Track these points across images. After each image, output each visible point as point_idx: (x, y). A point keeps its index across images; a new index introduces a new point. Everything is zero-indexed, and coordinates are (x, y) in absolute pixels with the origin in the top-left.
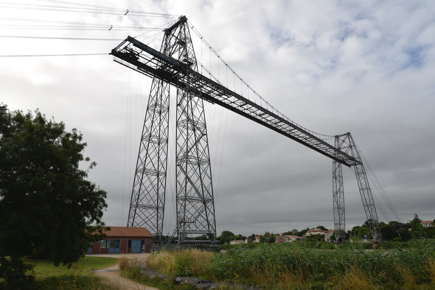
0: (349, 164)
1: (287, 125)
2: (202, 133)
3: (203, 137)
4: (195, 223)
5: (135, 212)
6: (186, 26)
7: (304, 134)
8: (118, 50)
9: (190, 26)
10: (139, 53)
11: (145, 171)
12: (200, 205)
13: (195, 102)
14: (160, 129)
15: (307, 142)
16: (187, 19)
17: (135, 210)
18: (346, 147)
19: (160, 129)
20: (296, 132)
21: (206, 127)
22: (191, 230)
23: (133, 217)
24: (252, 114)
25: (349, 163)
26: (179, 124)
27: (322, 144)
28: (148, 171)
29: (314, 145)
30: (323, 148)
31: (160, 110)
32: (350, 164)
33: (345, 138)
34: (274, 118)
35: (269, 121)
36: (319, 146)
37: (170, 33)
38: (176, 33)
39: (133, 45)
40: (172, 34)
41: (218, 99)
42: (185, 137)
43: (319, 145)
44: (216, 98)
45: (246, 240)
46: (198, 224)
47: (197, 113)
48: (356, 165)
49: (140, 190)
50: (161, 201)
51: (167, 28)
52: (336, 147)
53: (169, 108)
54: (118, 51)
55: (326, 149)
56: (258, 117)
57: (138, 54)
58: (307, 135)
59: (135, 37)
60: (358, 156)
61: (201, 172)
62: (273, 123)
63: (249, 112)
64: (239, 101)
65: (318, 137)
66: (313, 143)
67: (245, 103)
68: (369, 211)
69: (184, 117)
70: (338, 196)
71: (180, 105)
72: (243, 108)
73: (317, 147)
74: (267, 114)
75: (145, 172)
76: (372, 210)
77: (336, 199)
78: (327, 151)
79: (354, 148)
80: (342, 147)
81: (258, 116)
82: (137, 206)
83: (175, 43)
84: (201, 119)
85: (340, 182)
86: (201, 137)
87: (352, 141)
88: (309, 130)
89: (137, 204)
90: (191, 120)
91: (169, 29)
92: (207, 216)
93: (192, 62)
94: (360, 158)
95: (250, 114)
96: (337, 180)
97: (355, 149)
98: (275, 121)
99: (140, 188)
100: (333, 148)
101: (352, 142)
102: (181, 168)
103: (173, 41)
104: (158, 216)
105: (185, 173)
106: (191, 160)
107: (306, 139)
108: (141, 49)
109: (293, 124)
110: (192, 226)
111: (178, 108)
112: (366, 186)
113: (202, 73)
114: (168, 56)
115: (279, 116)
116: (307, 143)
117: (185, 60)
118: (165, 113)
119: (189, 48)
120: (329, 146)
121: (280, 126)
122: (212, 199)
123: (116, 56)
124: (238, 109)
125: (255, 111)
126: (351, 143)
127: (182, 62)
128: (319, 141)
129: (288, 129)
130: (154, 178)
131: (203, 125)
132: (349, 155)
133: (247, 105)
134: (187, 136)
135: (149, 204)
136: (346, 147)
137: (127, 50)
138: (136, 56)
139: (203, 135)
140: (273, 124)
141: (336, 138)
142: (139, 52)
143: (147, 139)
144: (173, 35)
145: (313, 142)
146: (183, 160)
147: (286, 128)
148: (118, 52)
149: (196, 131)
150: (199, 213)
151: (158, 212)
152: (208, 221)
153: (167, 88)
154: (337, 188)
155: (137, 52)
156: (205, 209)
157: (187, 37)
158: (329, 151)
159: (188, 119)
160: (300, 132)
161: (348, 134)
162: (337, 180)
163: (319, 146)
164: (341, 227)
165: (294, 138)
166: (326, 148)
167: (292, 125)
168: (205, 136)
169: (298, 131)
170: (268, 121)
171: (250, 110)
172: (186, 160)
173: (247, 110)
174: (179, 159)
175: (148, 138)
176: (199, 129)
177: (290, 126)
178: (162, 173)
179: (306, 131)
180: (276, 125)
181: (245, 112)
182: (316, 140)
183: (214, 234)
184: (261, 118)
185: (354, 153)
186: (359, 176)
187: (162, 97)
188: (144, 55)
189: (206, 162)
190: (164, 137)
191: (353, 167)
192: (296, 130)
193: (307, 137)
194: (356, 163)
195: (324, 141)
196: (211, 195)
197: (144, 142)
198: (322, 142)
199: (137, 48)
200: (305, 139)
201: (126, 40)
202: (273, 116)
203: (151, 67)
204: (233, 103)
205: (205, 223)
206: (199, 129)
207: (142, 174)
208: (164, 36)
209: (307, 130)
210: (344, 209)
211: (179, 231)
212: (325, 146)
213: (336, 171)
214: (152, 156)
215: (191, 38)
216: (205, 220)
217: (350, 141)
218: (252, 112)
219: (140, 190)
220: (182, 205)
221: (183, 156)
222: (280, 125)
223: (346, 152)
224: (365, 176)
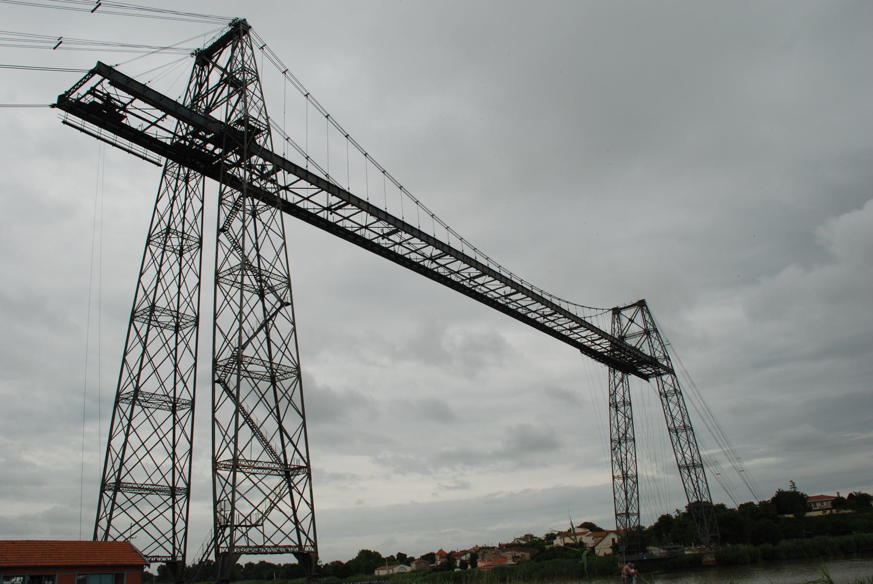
0: (645, 374)
1: (497, 282)
2: (281, 301)
3: (282, 310)
4: (260, 528)
5: (114, 503)
6: (248, 43)
7: (539, 304)
8: (74, 96)
9: (257, 44)
10: (125, 105)
11: (171, 405)
12: (274, 481)
13: (263, 223)
14: (179, 292)
15: (547, 324)
16: (250, 27)
17: (112, 498)
18: (637, 335)
19: (179, 292)
20: (521, 299)
21: (289, 286)
22: (251, 544)
23: (108, 516)
24: (413, 256)
25: (645, 370)
26: (221, 278)
27: (582, 328)
28: (147, 399)
29: (564, 330)
30: (585, 337)
31: (182, 246)
32: (647, 373)
33: (635, 313)
34: (466, 266)
35: (455, 272)
36: (577, 333)
37: (209, 61)
38: (223, 59)
39: (109, 83)
40: (212, 62)
41: (327, 218)
42: (237, 310)
43: (575, 331)
44: (321, 215)
45: (413, 565)
46: (268, 528)
47: (267, 252)
48: (660, 375)
49: (125, 445)
50: (180, 474)
51: (202, 48)
52: (616, 334)
53: (201, 239)
54: (74, 99)
55: (593, 339)
56: (427, 264)
57: (124, 107)
58: (547, 307)
59: (117, 65)
60: (664, 355)
61: (279, 397)
62: (464, 278)
63: (405, 251)
64: (380, 224)
65: (573, 310)
66: (561, 325)
67: (393, 229)
68: (692, 479)
69: (235, 260)
70: (623, 450)
71: (226, 230)
72: (389, 240)
73: (571, 336)
74: (448, 257)
75: (138, 400)
76: (697, 478)
77: (619, 456)
78: (596, 344)
79: (655, 335)
80: (627, 334)
81: (428, 261)
82: (118, 486)
83: (221, 81)
84: (278, 265)
85: (625, 416)
86: (278, 310)
87: (651, 319)
88: (550, 296)
89: (118, 481)
90: (254, 267)
91: (206, 49)
92: (293, 508)
93: (258, 127)
94: (669, 360)
95: (407, 256)
96: (619, 412)
97: (657, 338)
98: (469, 274)
99: (126, 441)
100: (609, 338)
101: (649, 321)
102: (226, 389)
103: (215, 77)
104: (174, 512)
105: (236, 399)
106: (250, 368)
107: (545, 316)
108: (129, 94)
109: (513, 279)
110: (253, 533)
111: (220, 238)
112: (684, 422)
113: (307, 167)
114: (201, 112)
115: (478, 260)
116: (548, 327)
117: (239, 122)
118: (192, 252)
119: (253, 94)
120: (598, 332)
121: (483, 285)
122: (305, 465)
123: (102, 128)
124: (410, 258)
125: (420, 249)
126: (648, 325)
127: (234, 125)
128: (539, 300)
129: (501, 291)
130: (163, 415)
131: (284, 280)
132: (644, 352)
133: (400, 233)
134: (241, 307)
135: (149, 482)
136: (637, 335)
137: (94, 97)
138: (119, 111)
139: (284, 304)
140: (465, 280)
141: (614, 314)
142: (126, 101)
143: (145, 317)
144: (215, 65)
145: (562, 324)
146: (231, 368)
147: (496, 291)
148: (74, 101)
149: (266, 296)
150: (273, 502)
151: (176, 501)
152: (297, 522)
153: (197, 192)
154: (620, 429)
155: (122, 103)
156: (288, 489)
157: (248, 67)
158: (599, 345)
159: (245, 264)
160: (530, 299)
161: (641, 304)
162: (619, 412)
163: (577, 333)
164: (631, 521)
165: (552, 332)
166: (591, 338)
167: (509, 282)
168: (289, 308)
169: (524, 296)
170: (452, 272)
171: (407, 246)
172: (236, 368)
173: (400, 247)
174: (221, 366)
175: (148, 313)
176: (272, 289)
177: (506, 285)
178: (183, 404)
179: (544, 296)
180: (472, 283)
181: (426, 266)
182: (569, 319)
183: (311, 554)
184: (434, 265)
185: (655, 347)
186: (667, 400)
187: (185, 212)
188: (139, 109)
189: (291, 372)
190: (190, 312)
191: (653, 380)
192: (519, 296)
193: (548, 311)
194: (661, 370)
195: (588, 320)
196: (304, 455)
197: (138, 325)
198: (583, 324)
199: (120, 92)
200: (542, 316)
201: (92, 73)
202: (475, 266)
203: (156, 138)
204: (364, 229)
205: (290, 526)
206: (272, 289)
207: (131, 405)
208: (195, 67)
209: (546, 294)
210: (637, 478)
211: (220, 549)
212: (589, 332)
213: (617, 390)
214: (156, 361)
215: (257, 70)
216: (289, 519)
217: (646, 321)
218: (412, 251)
219: (125, 445)
220: (227, 481)
221: (231, 357)
222: (481, 283)
223: (638, 347)
224: (681, 400)
